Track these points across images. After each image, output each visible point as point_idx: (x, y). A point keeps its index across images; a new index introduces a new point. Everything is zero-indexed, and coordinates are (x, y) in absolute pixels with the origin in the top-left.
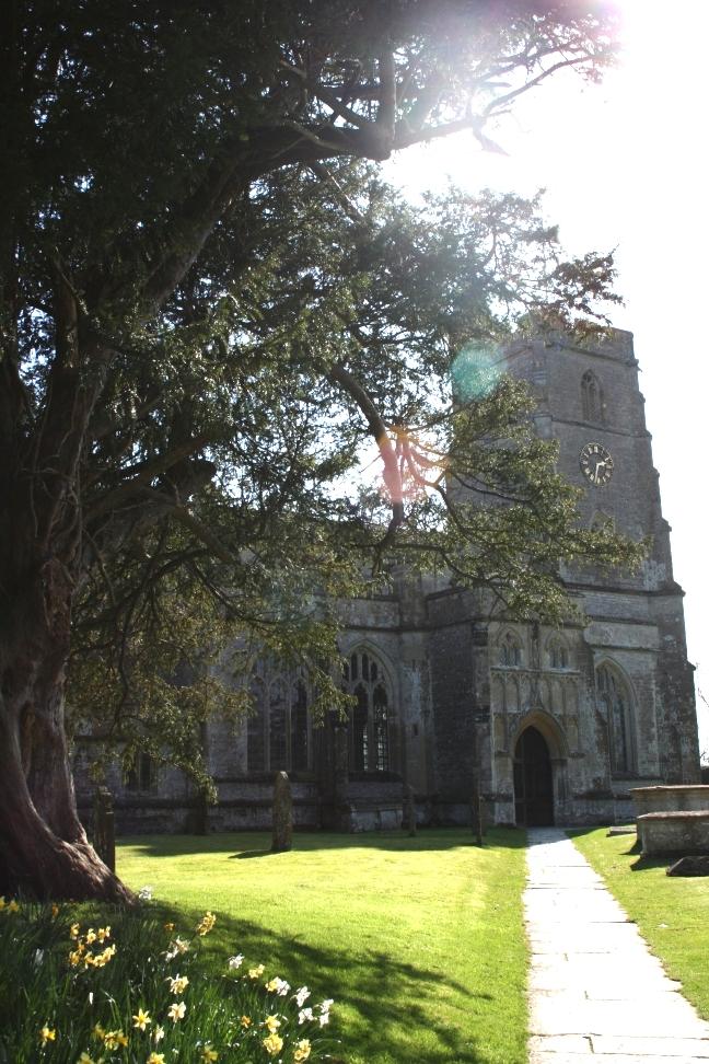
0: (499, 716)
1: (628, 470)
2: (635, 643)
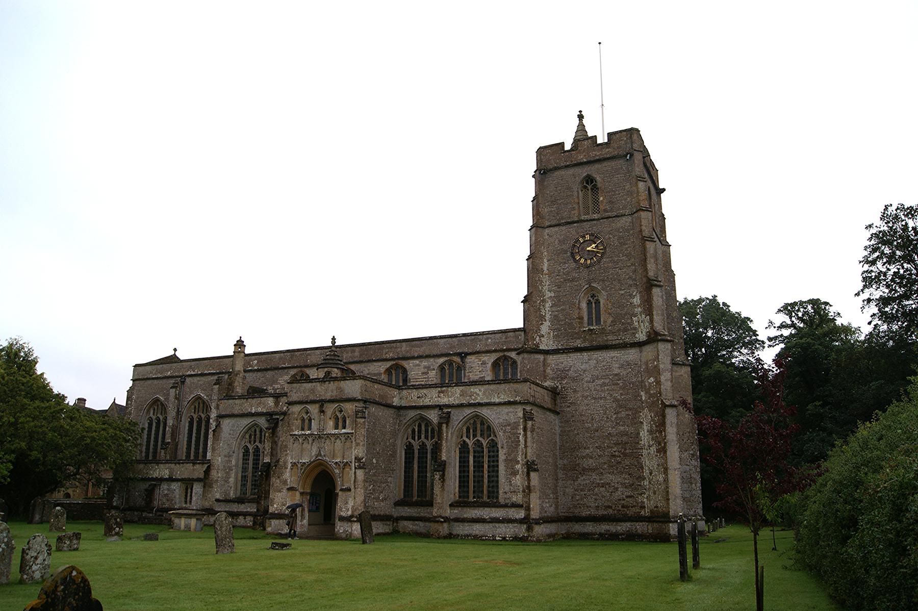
2: (504, 398)
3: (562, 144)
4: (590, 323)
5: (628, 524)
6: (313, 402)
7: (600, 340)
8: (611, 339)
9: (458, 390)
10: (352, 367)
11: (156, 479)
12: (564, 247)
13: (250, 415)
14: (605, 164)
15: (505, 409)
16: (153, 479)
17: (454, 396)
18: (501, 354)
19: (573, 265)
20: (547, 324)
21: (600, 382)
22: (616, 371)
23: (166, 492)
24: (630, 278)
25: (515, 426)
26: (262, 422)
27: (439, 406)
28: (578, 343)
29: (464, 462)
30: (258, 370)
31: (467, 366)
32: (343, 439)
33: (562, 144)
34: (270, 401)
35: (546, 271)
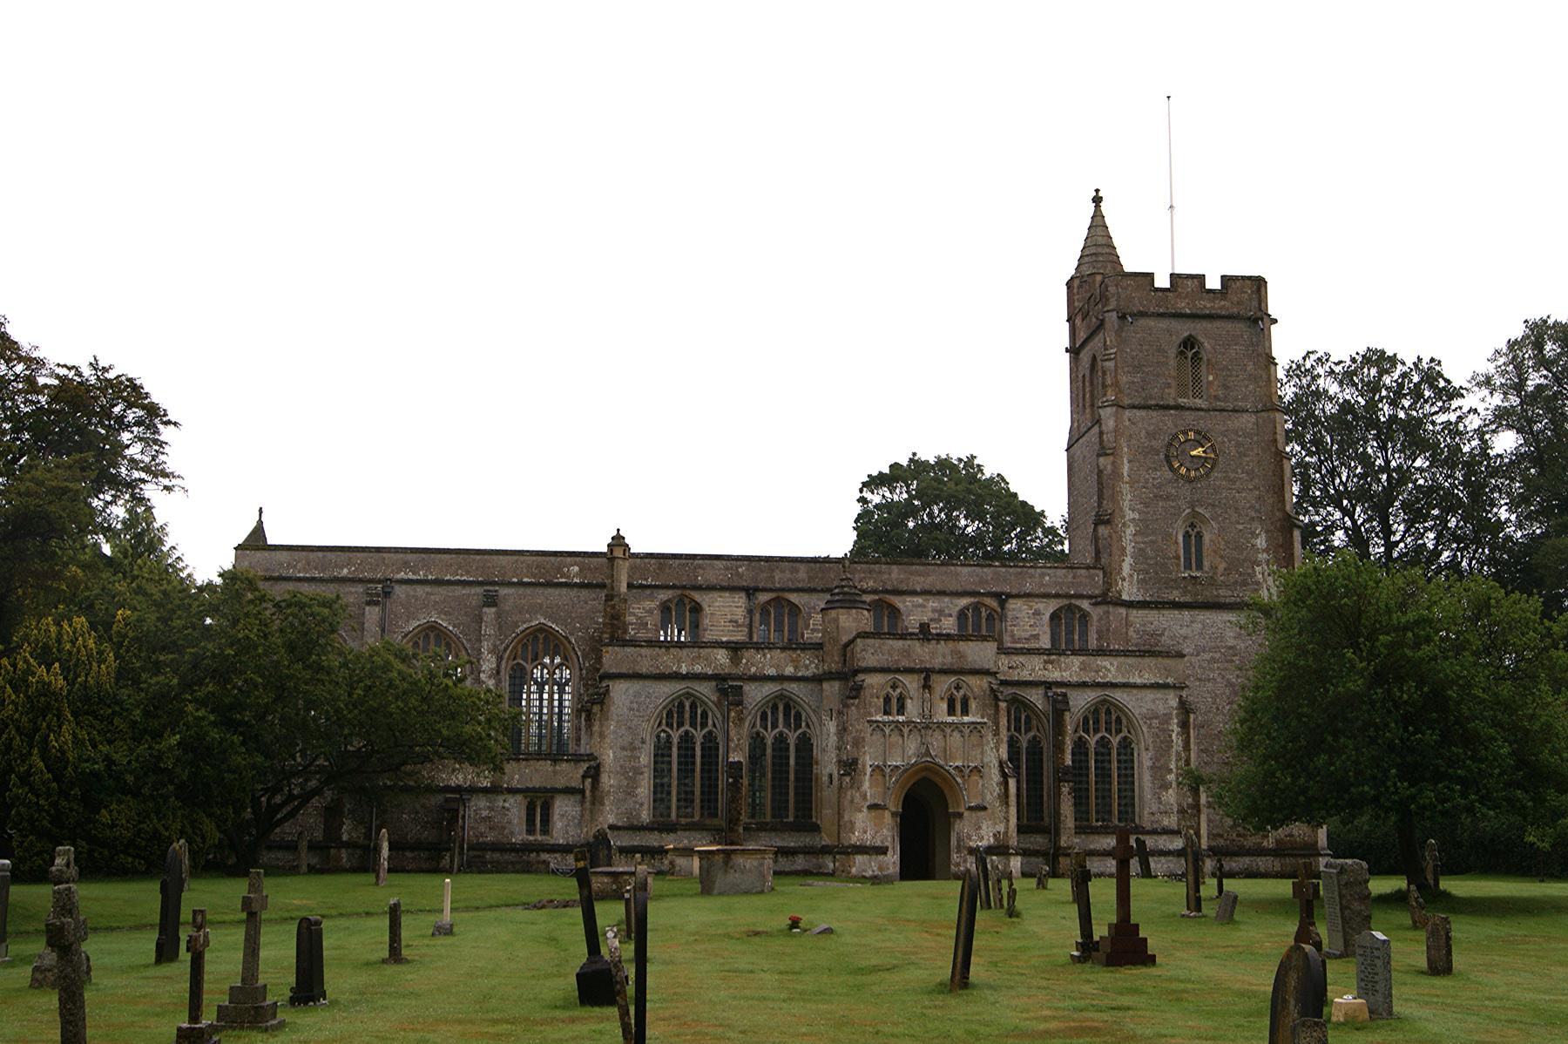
0: (877, 769)
1: (1242, 455)
2: (1148, 678)
3: (1150, 276)
4: (1188, 567)
5: (1247, 860)
6: (909, 671)
7: (1207, 595)
8: (1224, 595)
9: (1076, 661)
10: (794, 598)
11: (458, 789)
12: (1154, 443)
13: (676, 677)
14: (1218, 324)
15: (1150, 695)
16: (448, 789)
17: (1069, 669)
18: (1066, 602)
19: (1169, 475)
20: (1128, 560)
21: (1207, 656)
22: (1231, 642)
23: (485, 813)
24: (1252, 507)
25: (1166, 719)
26: (706, 690)
27: (1045, 683)
28: (1175, 595)
29: (686, 763)
30: (582, 586)
31: (1010, 614)
32: (967, 731)
33: (1150, 276)
34: (722, 656)
35: (1126, 479)
